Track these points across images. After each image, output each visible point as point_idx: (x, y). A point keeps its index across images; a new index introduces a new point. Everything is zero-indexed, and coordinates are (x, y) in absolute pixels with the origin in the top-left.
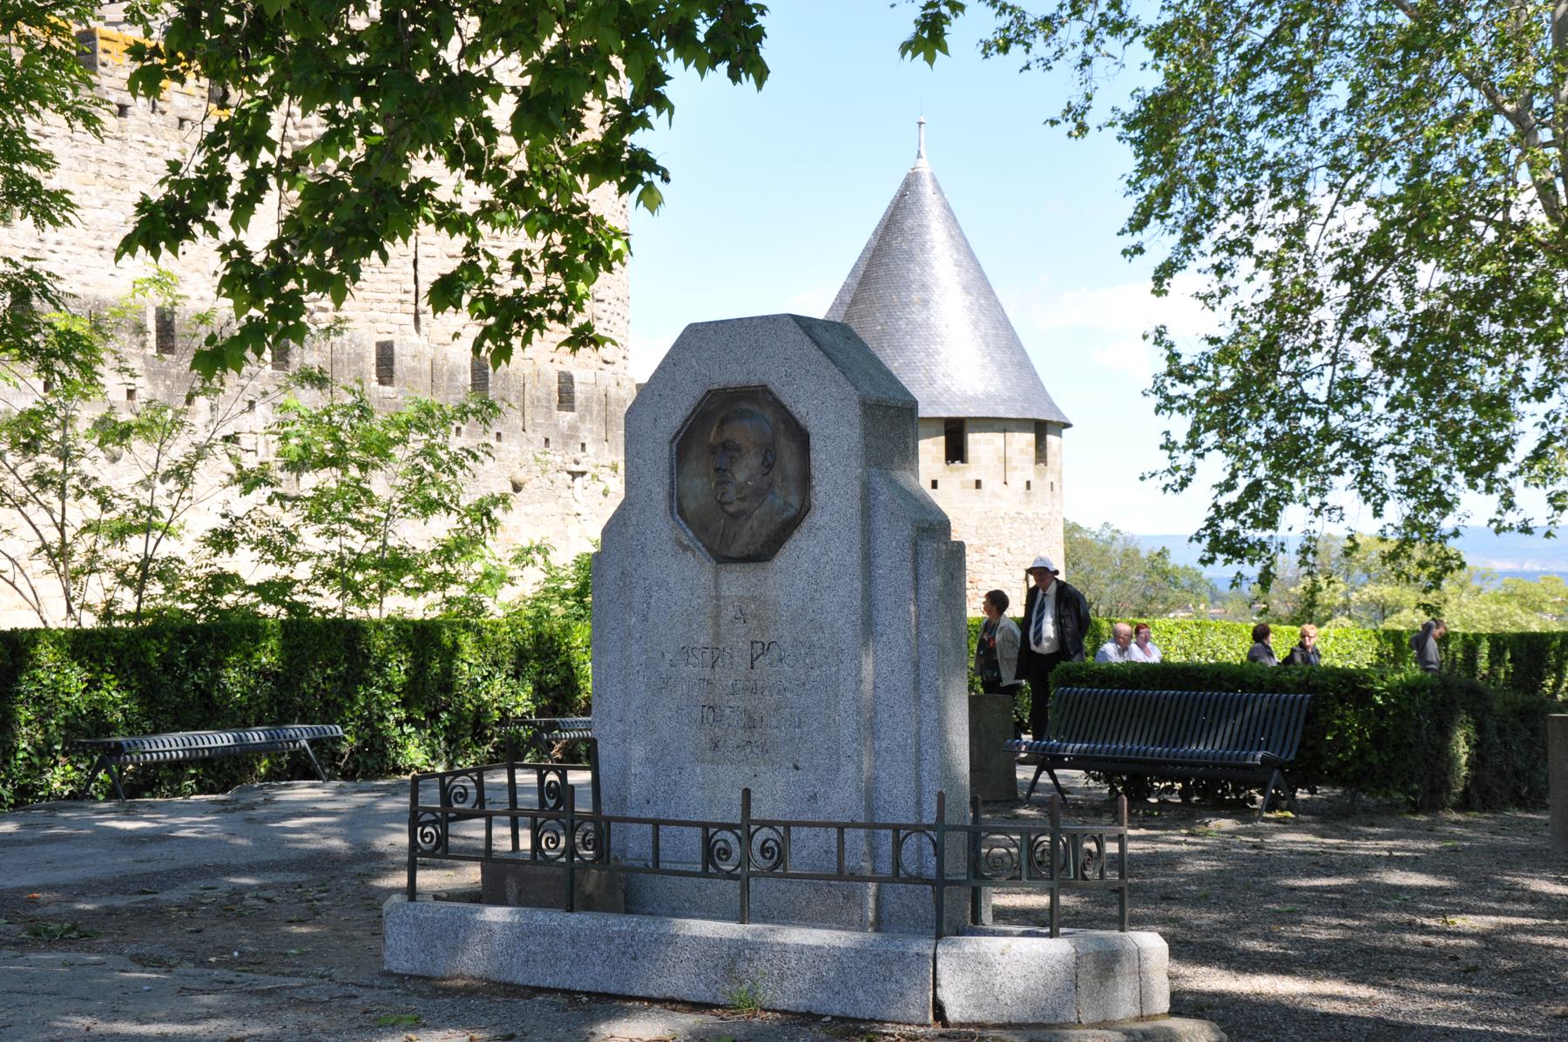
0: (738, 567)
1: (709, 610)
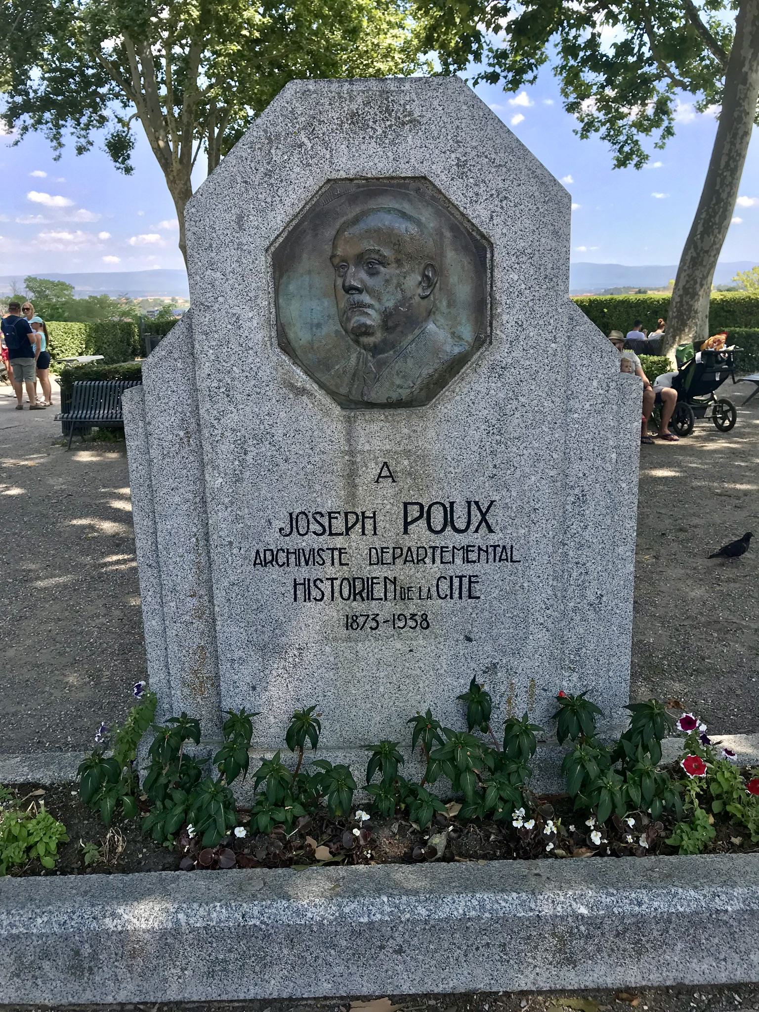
0: (377, 414)
1: (339, 467)
